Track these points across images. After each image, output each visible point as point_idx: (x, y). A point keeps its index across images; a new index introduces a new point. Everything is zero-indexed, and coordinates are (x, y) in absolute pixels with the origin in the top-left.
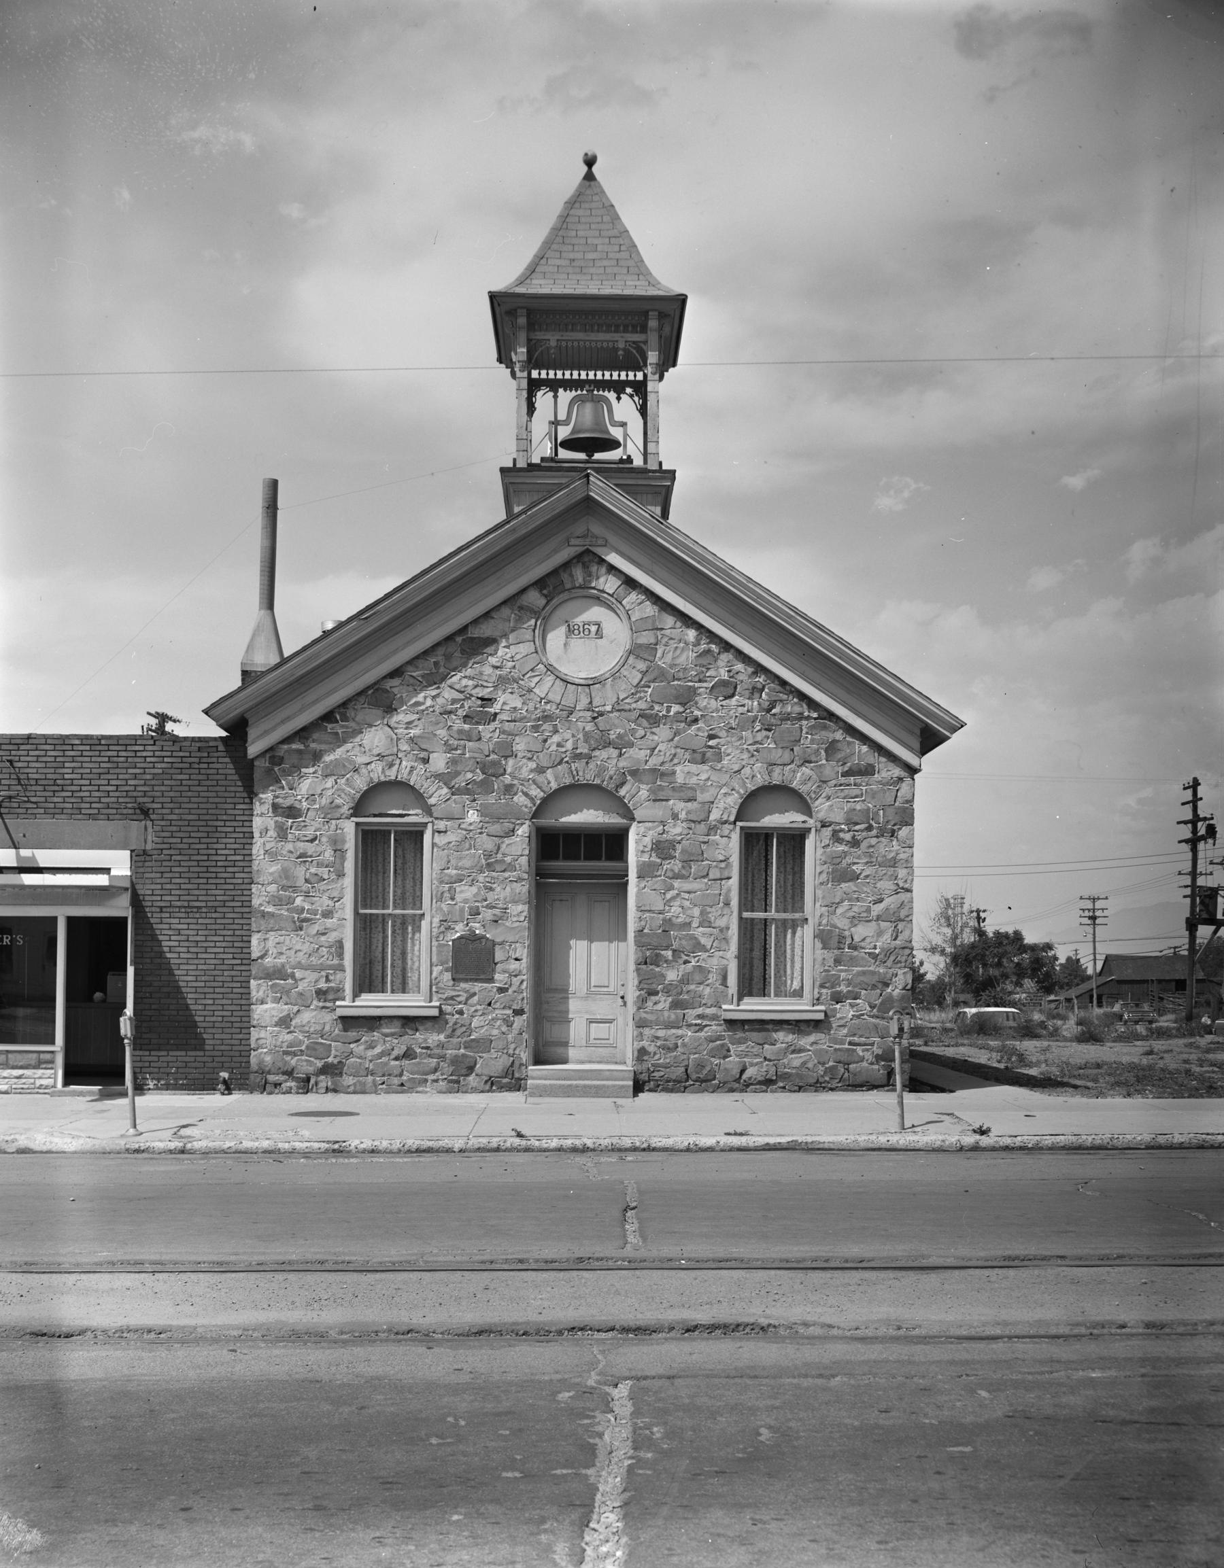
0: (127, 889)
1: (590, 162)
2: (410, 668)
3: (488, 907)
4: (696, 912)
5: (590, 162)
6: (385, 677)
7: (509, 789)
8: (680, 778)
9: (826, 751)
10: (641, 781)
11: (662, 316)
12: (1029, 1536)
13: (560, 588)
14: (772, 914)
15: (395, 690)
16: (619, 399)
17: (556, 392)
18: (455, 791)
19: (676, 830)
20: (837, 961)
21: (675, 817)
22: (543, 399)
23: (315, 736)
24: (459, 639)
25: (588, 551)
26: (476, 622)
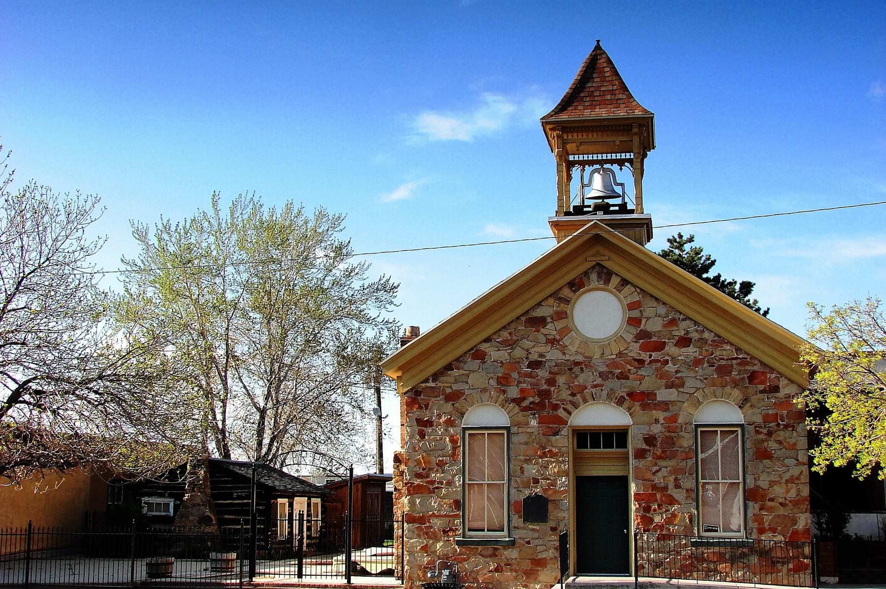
0: (381, 471)
1: (598, 41)
2: (495, 337)
3: (543, 479)
4: (672, 478)
5: (598, 41)
6: (481, 343)
7: (555, 407)
8: (659, 398)
9: (748, 378)
10: (634, 400)
11: (640, 126)
12: (104, 322)
13: (581, 285)
14: (720, 481)
15: (487, 350)
16: (621, 169)
17: (584, 167)
18: (525, 409)
19: (657, 429)
20: (761, 509)
21: (657, 421)
22: (576, 172)
23: (441, 379)
24: (523, 319)
25: (598, 264)
26: (533, 308)
